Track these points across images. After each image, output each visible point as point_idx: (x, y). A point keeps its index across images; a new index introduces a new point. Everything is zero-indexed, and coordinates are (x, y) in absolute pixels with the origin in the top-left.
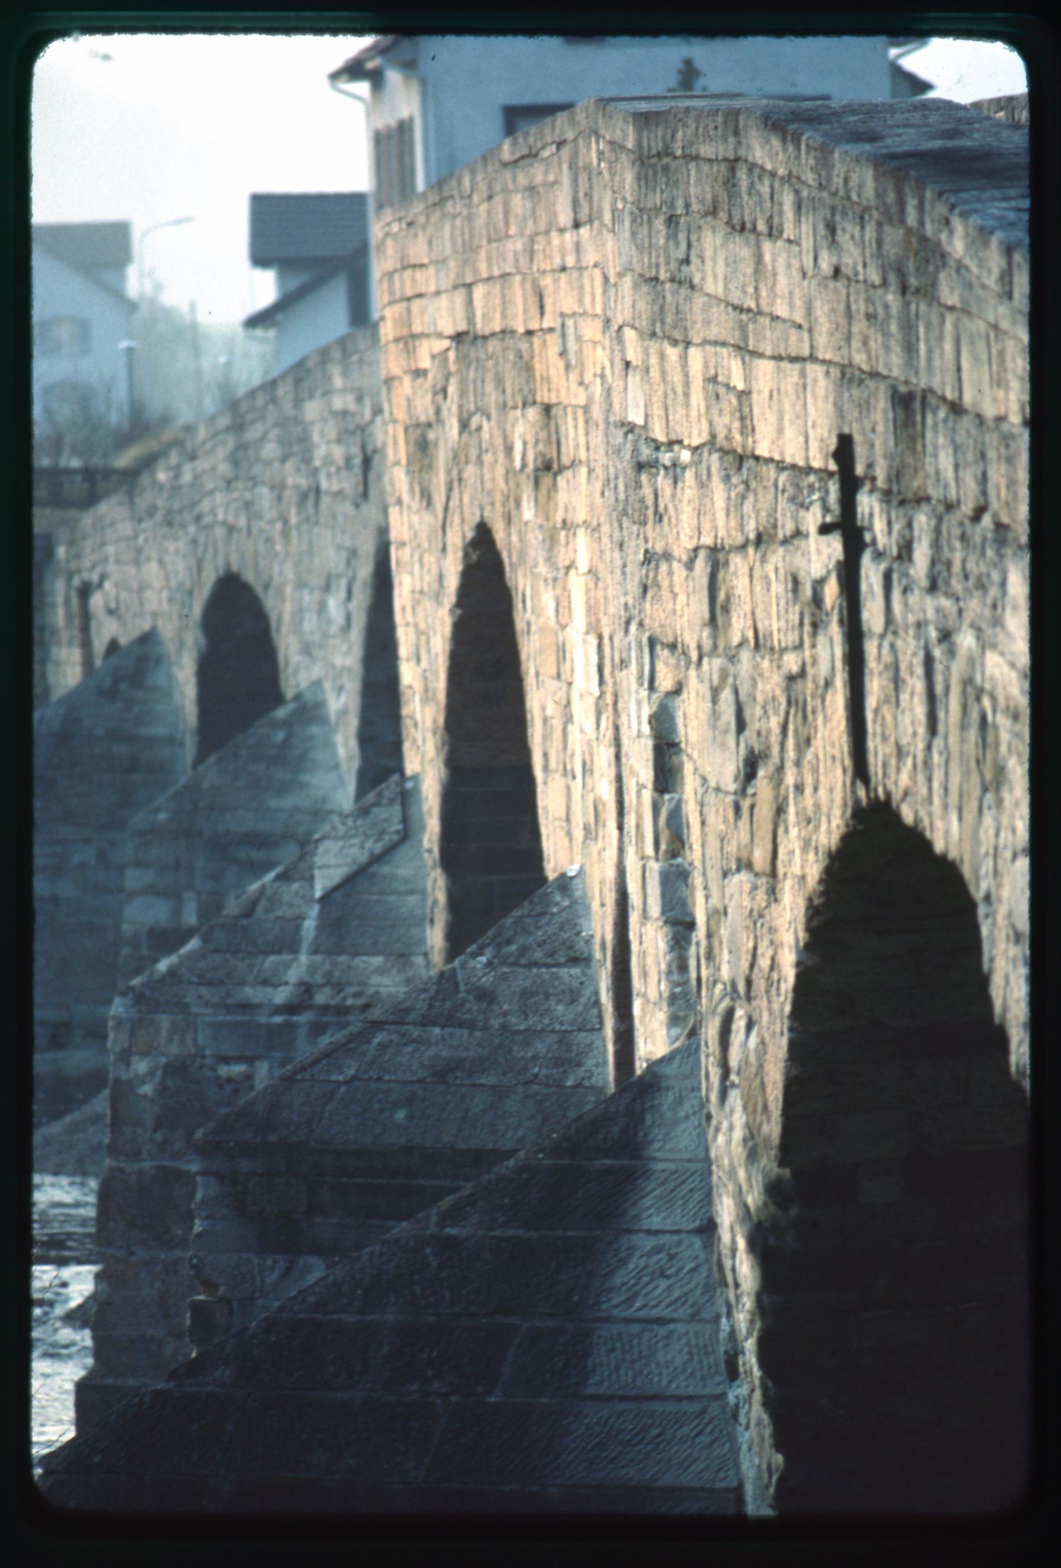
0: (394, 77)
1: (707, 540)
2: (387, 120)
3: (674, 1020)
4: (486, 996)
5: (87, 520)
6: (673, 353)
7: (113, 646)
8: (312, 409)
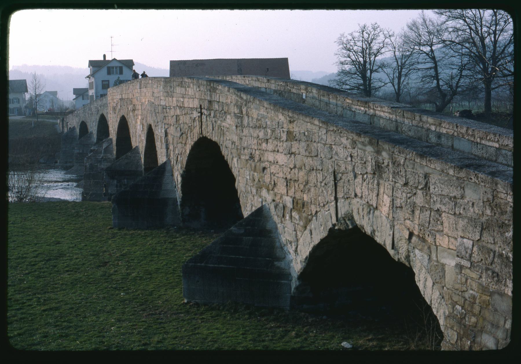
0: (91, 78)
1: (176, 114)
2: (90, 81)
3: (167, 157)
4: (130, 157)
5: (68, 116)
6: (170, 99)
7: (70, 128)
8: (92, 106)
